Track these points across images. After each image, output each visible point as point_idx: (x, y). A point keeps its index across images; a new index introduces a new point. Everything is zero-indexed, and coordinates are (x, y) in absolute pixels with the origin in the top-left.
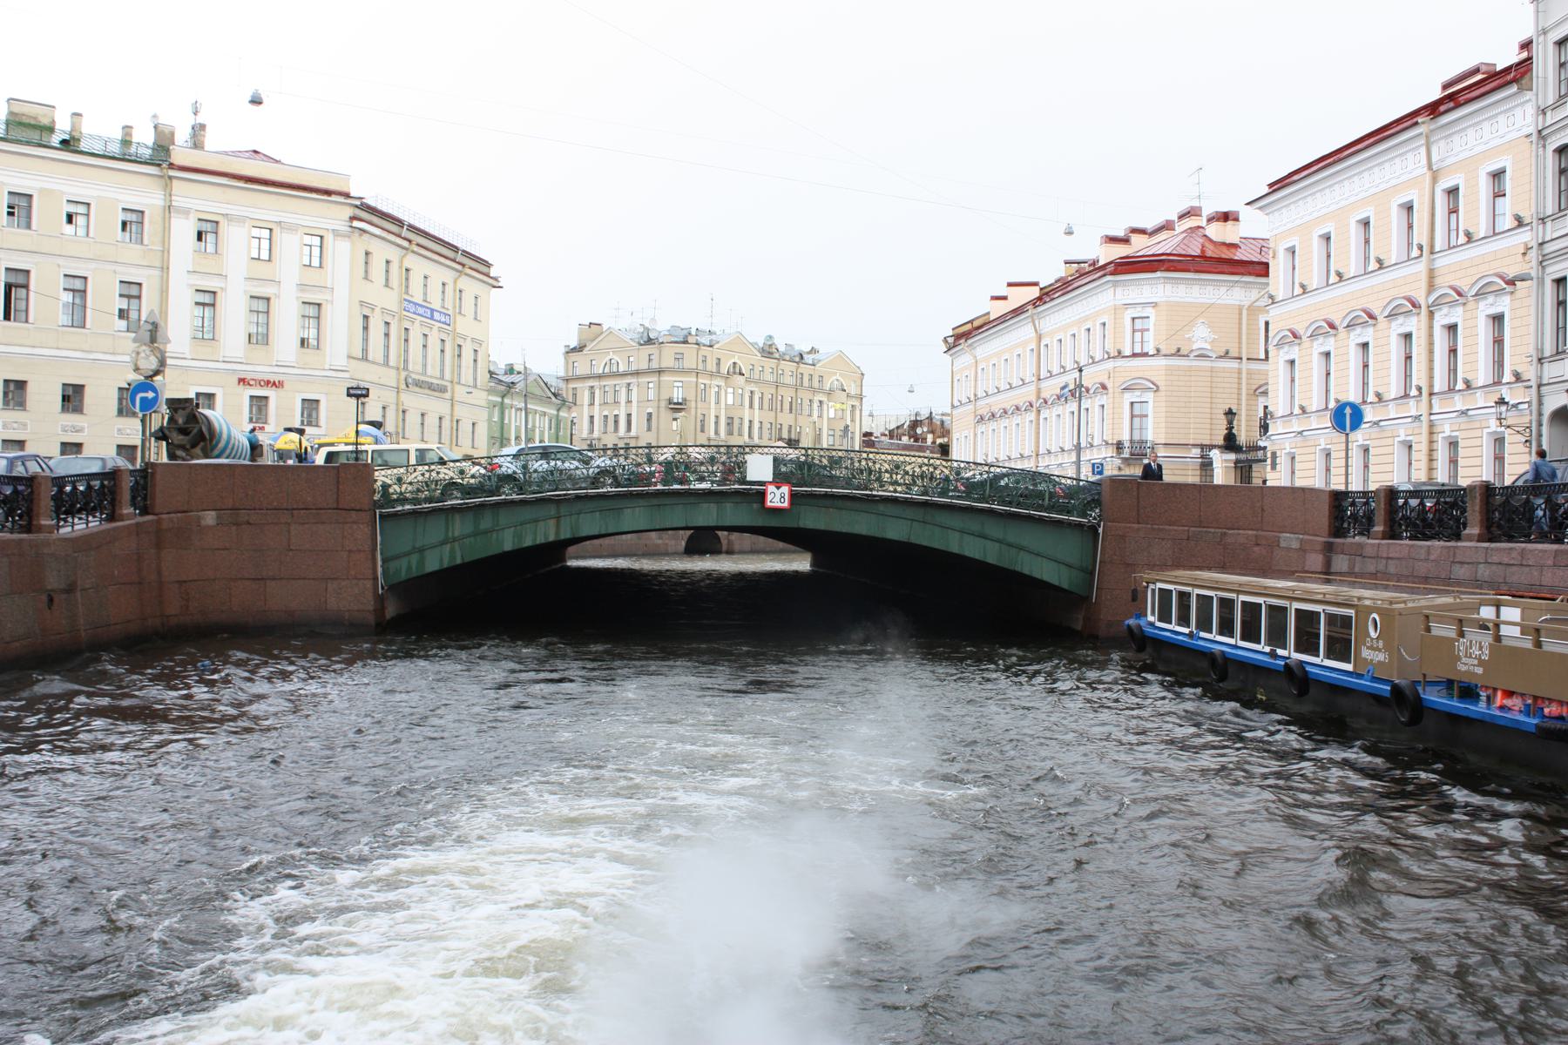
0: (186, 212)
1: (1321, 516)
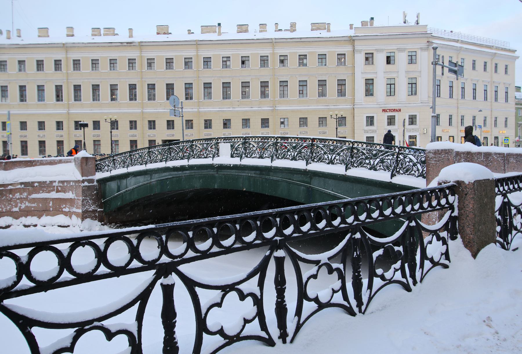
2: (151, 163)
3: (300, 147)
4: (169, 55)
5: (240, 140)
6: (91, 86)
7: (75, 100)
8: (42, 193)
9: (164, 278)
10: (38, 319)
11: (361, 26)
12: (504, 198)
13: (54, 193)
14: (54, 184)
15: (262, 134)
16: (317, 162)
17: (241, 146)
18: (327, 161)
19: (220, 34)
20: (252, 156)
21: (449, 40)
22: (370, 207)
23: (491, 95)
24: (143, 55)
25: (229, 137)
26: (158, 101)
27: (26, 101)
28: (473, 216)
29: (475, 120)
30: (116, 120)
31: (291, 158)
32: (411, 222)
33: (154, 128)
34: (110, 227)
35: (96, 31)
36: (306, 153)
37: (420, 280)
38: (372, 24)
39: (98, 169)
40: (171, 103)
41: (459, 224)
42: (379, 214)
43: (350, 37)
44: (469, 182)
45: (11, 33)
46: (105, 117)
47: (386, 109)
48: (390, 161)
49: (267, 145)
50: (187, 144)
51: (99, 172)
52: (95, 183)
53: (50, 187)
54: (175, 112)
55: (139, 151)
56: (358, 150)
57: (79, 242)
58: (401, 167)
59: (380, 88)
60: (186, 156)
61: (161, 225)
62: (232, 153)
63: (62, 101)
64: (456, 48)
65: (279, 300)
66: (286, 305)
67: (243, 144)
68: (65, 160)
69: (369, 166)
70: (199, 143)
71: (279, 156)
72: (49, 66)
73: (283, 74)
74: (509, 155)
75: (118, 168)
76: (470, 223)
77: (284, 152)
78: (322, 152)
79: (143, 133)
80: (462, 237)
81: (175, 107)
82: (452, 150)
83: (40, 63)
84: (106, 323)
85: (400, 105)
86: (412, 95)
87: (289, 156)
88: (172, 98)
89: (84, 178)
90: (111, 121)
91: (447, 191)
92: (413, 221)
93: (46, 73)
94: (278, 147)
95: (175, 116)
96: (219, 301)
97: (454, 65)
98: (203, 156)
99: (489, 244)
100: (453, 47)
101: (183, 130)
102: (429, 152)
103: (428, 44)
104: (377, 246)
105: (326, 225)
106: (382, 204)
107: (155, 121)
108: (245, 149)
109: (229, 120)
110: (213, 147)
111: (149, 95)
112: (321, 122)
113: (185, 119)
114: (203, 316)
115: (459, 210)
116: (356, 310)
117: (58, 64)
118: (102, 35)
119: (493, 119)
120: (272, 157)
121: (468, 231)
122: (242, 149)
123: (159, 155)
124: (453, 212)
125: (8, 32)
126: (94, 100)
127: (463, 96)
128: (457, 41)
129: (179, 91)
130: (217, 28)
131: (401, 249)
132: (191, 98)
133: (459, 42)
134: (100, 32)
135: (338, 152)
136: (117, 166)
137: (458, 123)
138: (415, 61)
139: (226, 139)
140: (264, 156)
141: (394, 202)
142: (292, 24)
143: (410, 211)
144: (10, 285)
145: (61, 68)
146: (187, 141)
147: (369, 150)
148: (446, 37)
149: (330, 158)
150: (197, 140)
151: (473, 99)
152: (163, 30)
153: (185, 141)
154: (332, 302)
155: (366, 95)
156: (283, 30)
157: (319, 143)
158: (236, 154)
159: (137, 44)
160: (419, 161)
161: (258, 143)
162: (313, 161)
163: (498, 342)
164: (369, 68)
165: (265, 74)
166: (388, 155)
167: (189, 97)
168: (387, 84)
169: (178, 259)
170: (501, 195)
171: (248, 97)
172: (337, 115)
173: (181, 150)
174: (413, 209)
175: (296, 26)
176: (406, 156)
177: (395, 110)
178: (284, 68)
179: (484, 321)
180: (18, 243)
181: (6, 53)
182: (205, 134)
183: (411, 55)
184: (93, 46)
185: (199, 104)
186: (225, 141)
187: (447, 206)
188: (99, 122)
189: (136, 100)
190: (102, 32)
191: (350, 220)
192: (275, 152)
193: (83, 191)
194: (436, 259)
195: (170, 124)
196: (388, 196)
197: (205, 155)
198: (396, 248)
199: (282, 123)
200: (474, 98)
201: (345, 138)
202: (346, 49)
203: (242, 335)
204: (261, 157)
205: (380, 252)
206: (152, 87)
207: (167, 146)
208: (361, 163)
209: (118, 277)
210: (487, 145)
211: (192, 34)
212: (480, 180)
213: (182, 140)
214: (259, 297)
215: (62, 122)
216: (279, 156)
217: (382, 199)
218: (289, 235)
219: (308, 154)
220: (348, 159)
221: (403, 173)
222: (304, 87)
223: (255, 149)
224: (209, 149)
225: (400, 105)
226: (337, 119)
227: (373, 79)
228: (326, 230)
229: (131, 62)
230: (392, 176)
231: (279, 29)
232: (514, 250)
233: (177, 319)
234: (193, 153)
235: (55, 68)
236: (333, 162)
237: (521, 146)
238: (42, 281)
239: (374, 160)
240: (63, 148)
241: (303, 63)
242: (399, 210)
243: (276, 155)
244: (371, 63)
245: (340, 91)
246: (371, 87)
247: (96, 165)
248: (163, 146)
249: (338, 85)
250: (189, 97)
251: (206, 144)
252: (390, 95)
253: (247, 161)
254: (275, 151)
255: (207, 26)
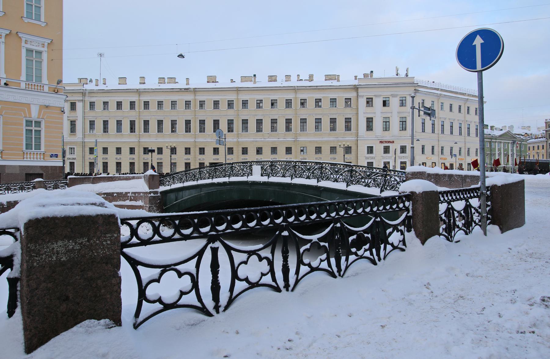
0: (362, 96)
1: (36, 187)
2: (201, 180)
3: (313, 169)
4: (216, 98)
5: (268, 163)
6: (157, 121)
7: (144, 132)
8: (120, 201)
9: (213, 243)
10: (142, 261)
11: (363, 77)
12: (449, 205)
13: (128, 201)
14: (128, 195)
15: (286, 159)
16: (325, 180)
17: (269, 168)
18: (333, 180)
19: (255, 82)
20: (277, 175)
21: (432, 88)
22: (347, 207)
23: (464, 131)
24: (196, 98)
25: (275, 161)
26: (207, 133)
27: (108, 132)
28: (422, 216)
29: (452, 150)
30: (175, 147)
31: (306, 178)
32: (377, 218)
33: (204, 154)
34: (169, 228)
35: (162, 80)
36: (346, 176)
37: (383, 258)
38: (371, 76)
39: (161, 184)
40: (216, 134)
41: (412, 221)
42: (354, 211)
43: (355, 85)
44: (419, 193)
45: (99, 81)
46: (167, 145)
47: (383, 141)
48: (380, 180)
49: (288, 168)
50: (228, 166)
51: (162, 186)
52: (159, 194)
53: (125, 197)
54: (220, 142)
55: (195, 170)
56: (356, 172)
57: (165, 218)
58: (388, 185)
59: (378, 124)
60: (227, 175)
61: (212, 212)
62: (262, 173)
63: (135, 132)
64: (437, 94)
65: (284, 263)
66: (289, 266)
67: (270, 166)
68: (137, 176)
69: (364, 184)
70: (237, 165)
71: (297, 176)
72: (126, 106)
73: (303, 113)
74: (466, 176)
75: (176, 183)
76: (420, 220)
77: (301, 172)
78: (330, 173)
79: (195, 157)
80: (414, 230)
81: (220, 138)
82: (424, 172)
83: (119, 104)
84: (178, 267)
85: (393, 138)
86: (403, 130)
87: (305, 175)
88: (218, 131)
89: (151, 190)
90: (171, 148)
91: (404, 199)
92: (379, 218)
93: (123, 111)
94: (296, 169)
95: (220, 144)
96: (245, 260)
97: (428, 109)
98: (240, 175)
99: (434, 235)
100: (435, 94)
101: (225, 155)
102: (408, 174)
103: (415, 91)
104: (353, 233)
105: (316, 217)
106: (356, 205)
107: (204, 148)
108: (272, 170)
109: (261, 148)
110: (248, 168)
111: (200, 129)
112: (332, 151)
113: (227, 147)
114: (236, 268)
115: (412, 211)
116: (337, 274)
117: (132, 105)
118: (166, 83)
119: (467, 150)
120: (292, 176)
121: (419, 226)
122: (270, 170)
123: (207, 174)
124: (408, 213)
125: (97, 80)
126: (158, 132)
127: (443, 132)
128: (438, 89)
129: (223, 126)
130: (253, 78)
131: (369, 236)
132: (232, 131)
133: (439, 90)
134: (165, 81)
135: (341, 173)
136: (176, 182)
137: (439, 152)
138: (405, 104)
139: (258, 162)
140: (286, 175)
141: (364, 204)
142: (310, 75)
143: (376, 211)
144: (127, 240)
145: (135, 107)
146: (229, 163)
147: (364, 172)
148: (429, 86)
149: (335, 177)
150: (236, 163)
151: (450, 133)
152: (212, 79)
153: (227, 164)
154: (320, 267)
155: (367, 130)
156: (303, 80)
157: (357, 169)
158: (265, 173)
159: (192, 90)
160: (401, 180)
161: (281, 165)
162: (323, 179)
163: (431, 298)
164: (370, 109)
165: (289, 113)
166: (378, 176)
167: (230, 130)
168: (383, 122)
169: (221, 233)
170: (446, 203)
171: (276, 131)
172: (344, 145)
173: (224, 170)
174: (378, 209)
175: (313, 77)
176: (392, 177)
177: (389, 141)
178: (303, 108)
179: (425, 285)
180: (132, 217)
181: (94, 96)
182: (242, 158)
183: (402, 99)
184: (159, 91)
185: (238, 136)
186: (257, 164)
187: (404, 208)
188: (162, 148)
189: (190, 132)
190: (166, 81)
191: (333, 214)
192: (294, 172)
193: (150, 200)
194: (396, 244)
195: (216, 151)
196: (360, 200)
197: (242, 174)
198: (366, 235)
199: (302, 151)
200: (452, 133)
201: (351, 163)
202: (352, 95)
203: (260, 282)
204: (284, 176)
205: (355, 237)
206: (202, 122)
207: (213, 167)
208: (358, 181)
209: (186, 241)
210: (470, 170)
211: (234, 82)
212: (427, 191)
213: (225, 163)
214: (272, 260)
215: (134, 148)
216: (297, 176)
217: (356, 202)
218: (291, 222)
219: (319, 174)
220: (348, 178)
221: (389, 189)
222: (319, 123)
223: (279, 170)
224: (245, 169)
225: (393, 138)
226: (344, 148)
227: (372, 118)
228: (317, 220)
229: (188, 104)
230: (382, 191)
231: (300, 79)
232: (456, 242)
233: (219, 269)
234: (233, 173)
235: (130, 107)
236: (369, 185)
237: (488, 171)
238: (144, 240)
239: (368, 180)
240: (134, 168)
241: (318, 104)
242: (368, 210)
243: (295, 175)
244: (371, 105)
245: (347, 127)
246: (371, 124)
247: (160, 181)
248: (210, 167)
249: (345, 122)
250: (230, 130)
251: (242, 166)
252: (386, 130)
253: (273, 179)
254: (294, 171)
255: (246, 77)
